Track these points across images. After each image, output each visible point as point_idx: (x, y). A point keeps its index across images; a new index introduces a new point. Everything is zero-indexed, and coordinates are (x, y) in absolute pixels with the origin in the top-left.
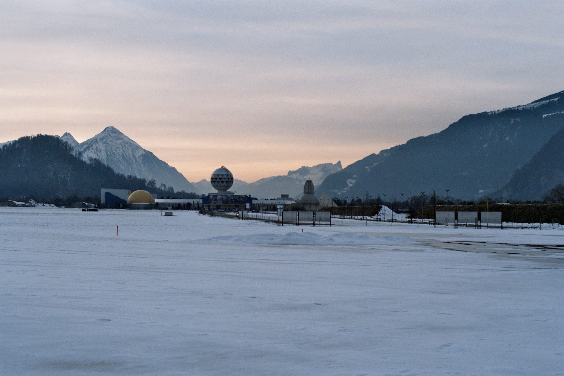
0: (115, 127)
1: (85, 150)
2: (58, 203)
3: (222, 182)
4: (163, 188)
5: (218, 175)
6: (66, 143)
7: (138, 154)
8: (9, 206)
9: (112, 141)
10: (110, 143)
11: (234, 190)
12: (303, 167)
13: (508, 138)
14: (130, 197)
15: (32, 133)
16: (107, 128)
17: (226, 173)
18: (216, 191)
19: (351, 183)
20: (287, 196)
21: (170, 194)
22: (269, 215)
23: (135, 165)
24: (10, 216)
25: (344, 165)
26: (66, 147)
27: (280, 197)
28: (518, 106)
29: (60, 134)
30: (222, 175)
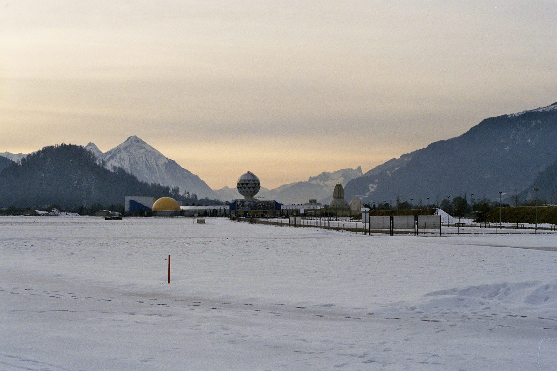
0: (138, 136)
1: (108, 160)
2: (82, 212)
3: (249, 188)
4: (186, 195)
5: (245, 181)
6: (90, 152)
7: (161, 162)
8: (32, 215)
9: (135, 150)
10: (134, 152)
11: (258, 197)
12: (324, 173)
13: (529, 140)
14: (154, 205)
15: (56, 141)
16: (130, 138)
17: (252, 178)
18: (242, 198)
19: (372, 188)
20: (315, 201)
21: (193, 201)
22: (281, 220)
23: (158, 174)
24: (20, 226)
25: (365, 171)
26: (89, 156)
27: (308, 202)
28: (538, 109)
29: (84, 145)
30: (249, 181)
